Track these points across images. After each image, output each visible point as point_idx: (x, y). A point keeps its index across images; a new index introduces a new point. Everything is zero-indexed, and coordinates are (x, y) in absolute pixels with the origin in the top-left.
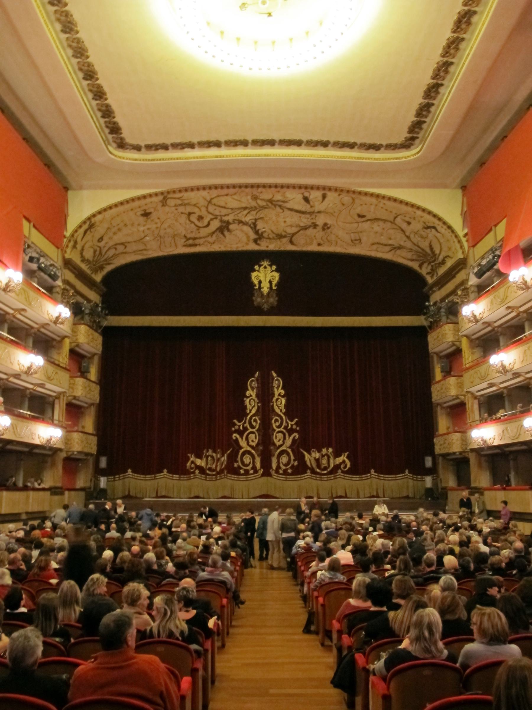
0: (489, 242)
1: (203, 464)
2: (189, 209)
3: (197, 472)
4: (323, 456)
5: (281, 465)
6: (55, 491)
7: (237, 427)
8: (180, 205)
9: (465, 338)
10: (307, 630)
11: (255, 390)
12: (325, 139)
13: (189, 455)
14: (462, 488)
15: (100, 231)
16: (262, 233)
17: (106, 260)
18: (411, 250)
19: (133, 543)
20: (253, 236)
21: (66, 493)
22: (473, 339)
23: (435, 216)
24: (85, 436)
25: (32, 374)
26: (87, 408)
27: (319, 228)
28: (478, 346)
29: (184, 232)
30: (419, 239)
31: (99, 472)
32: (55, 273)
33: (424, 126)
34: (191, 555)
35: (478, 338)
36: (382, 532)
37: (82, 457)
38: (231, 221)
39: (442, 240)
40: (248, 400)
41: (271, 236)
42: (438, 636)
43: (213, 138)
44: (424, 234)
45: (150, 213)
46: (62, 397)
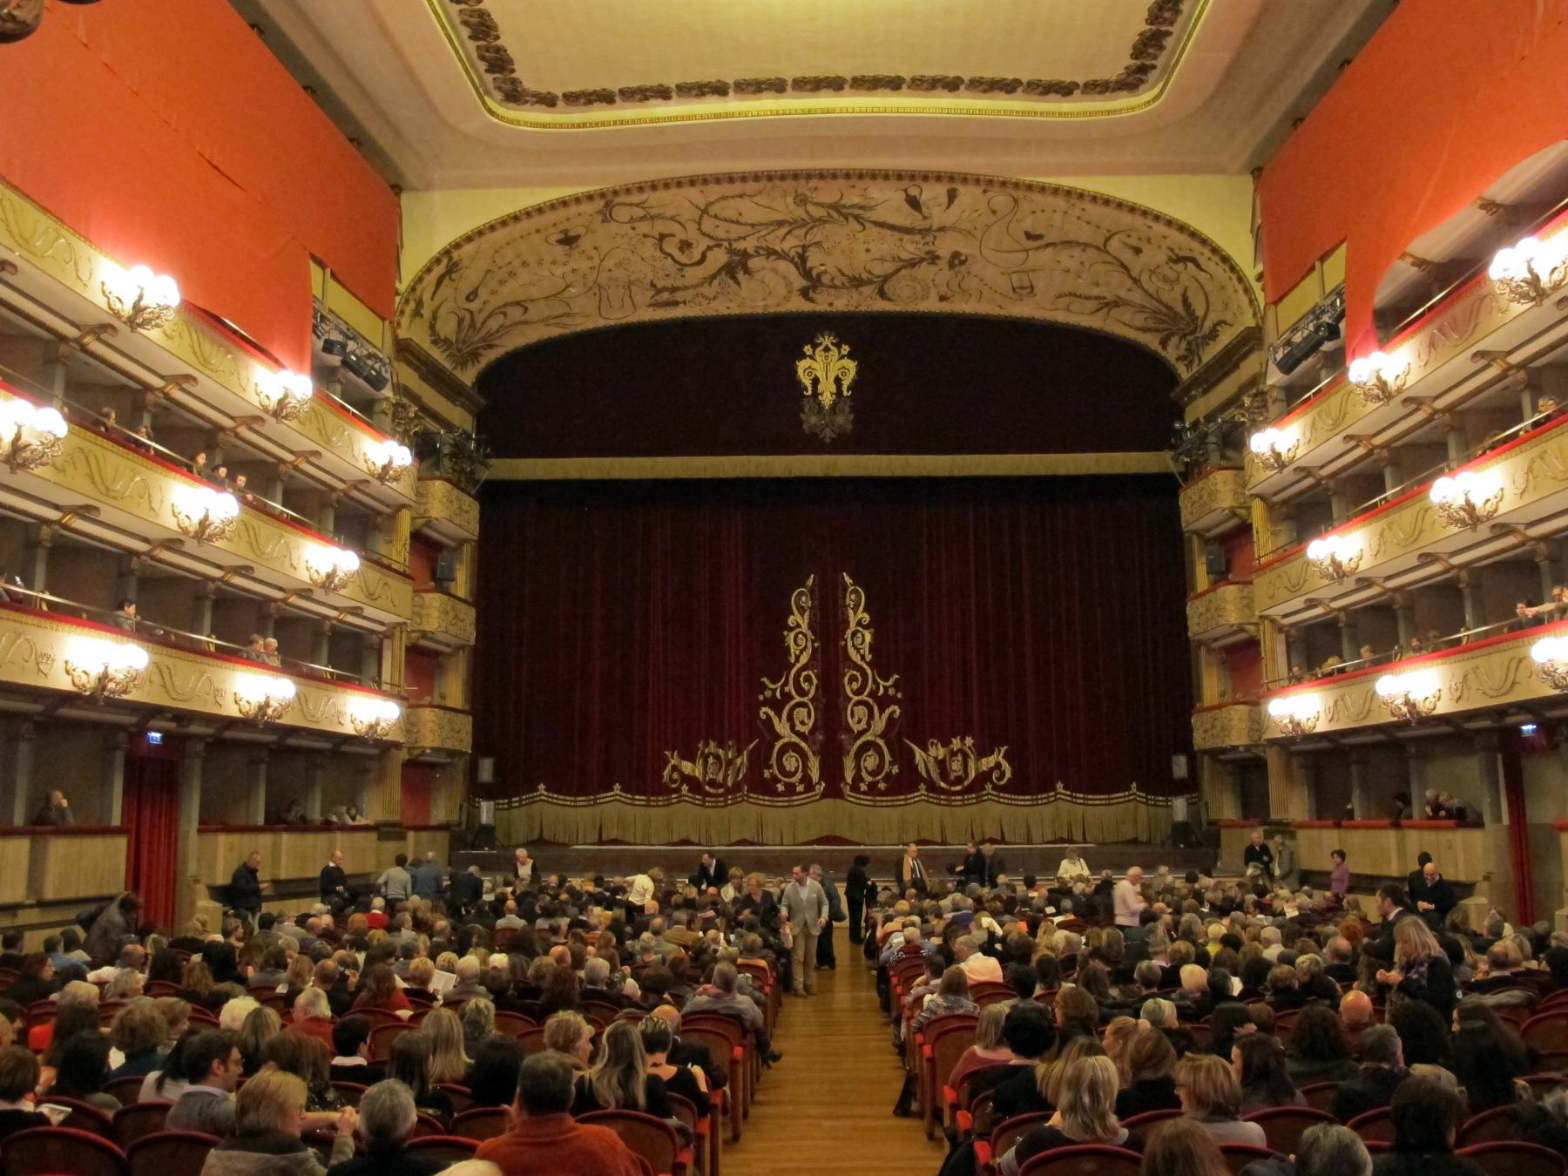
0: (1308, 294)
1: (698, 773)
2: (661, 227)
3: (685, 788)
4: (953, 754)
5: (864, 774)
6: (387, 831)
7: (768, 694)
8: (642, 219)
9: (1257, 501)
10: (902, 1110)
11: (806, 615)
12: (951, 74)
13: (668, 753)
14: (1251, 821)
15: (469, 278)
16: (819, 275)
17: (484, 339)
18: (1142, 308)
19: (553, 939)
20: (799, 282)
21: (411, 835)
22: (1275, 504)
23: (1193, 235)
24: (449, 715)
25: (335, 589)
26: (450, 655)
27: (943, 263)
28: (1287, 518)
29: (650, 277)
30: (1160, 284)
31: (476, 791)
32: (379, 373)
33: (1168, 43)
34: (676, 963)
35: (1285, 502)
36: (1072, 917)
37: (442, 759)
38: (751, 251)
39: (1209, 288)
40: (792, 635)
41: (838, 282)
42: (1108, 1104)
43: (709, 76)
44: (1172, 275)
45: (577, 237)
46: (397, 633)
